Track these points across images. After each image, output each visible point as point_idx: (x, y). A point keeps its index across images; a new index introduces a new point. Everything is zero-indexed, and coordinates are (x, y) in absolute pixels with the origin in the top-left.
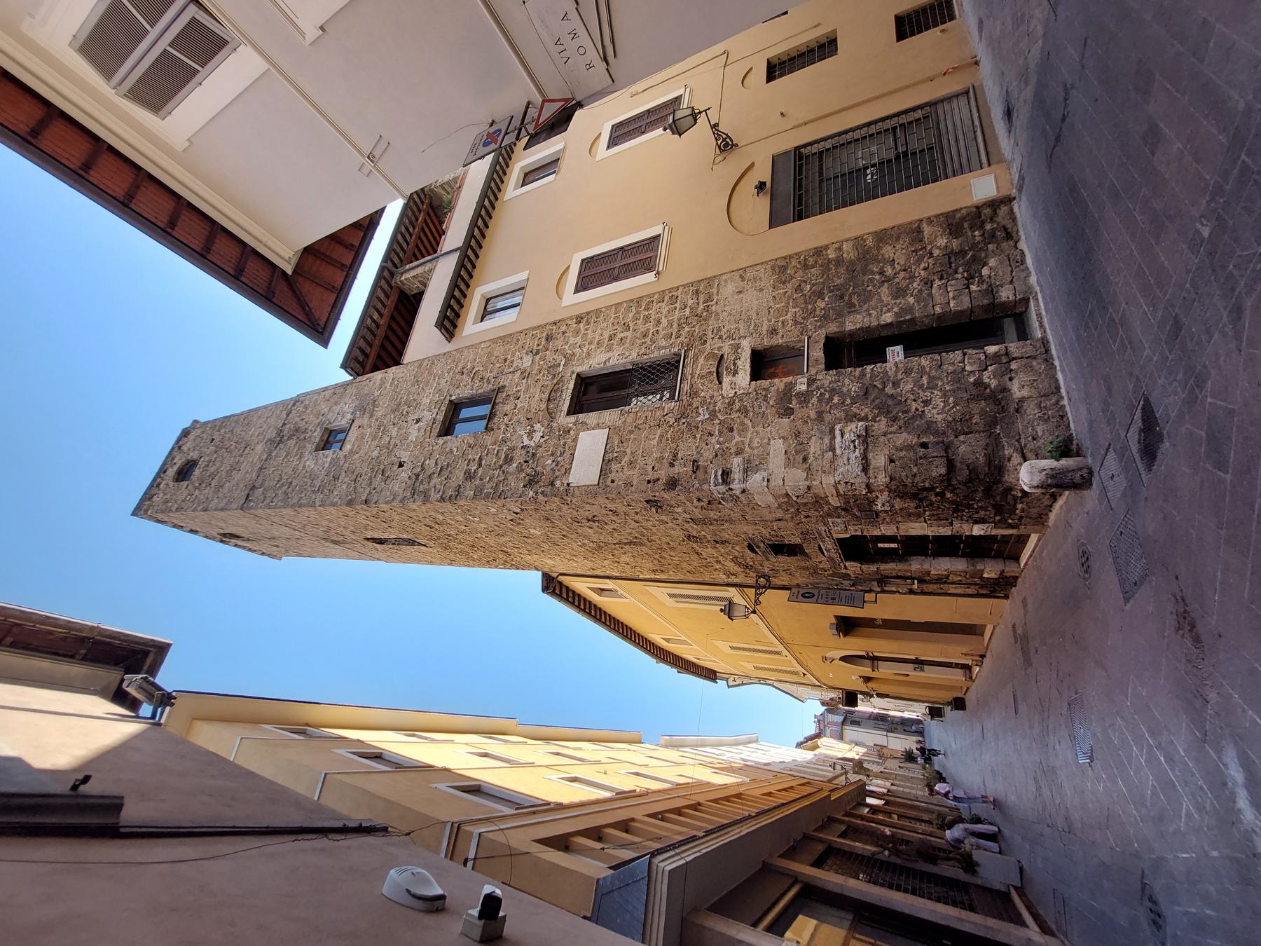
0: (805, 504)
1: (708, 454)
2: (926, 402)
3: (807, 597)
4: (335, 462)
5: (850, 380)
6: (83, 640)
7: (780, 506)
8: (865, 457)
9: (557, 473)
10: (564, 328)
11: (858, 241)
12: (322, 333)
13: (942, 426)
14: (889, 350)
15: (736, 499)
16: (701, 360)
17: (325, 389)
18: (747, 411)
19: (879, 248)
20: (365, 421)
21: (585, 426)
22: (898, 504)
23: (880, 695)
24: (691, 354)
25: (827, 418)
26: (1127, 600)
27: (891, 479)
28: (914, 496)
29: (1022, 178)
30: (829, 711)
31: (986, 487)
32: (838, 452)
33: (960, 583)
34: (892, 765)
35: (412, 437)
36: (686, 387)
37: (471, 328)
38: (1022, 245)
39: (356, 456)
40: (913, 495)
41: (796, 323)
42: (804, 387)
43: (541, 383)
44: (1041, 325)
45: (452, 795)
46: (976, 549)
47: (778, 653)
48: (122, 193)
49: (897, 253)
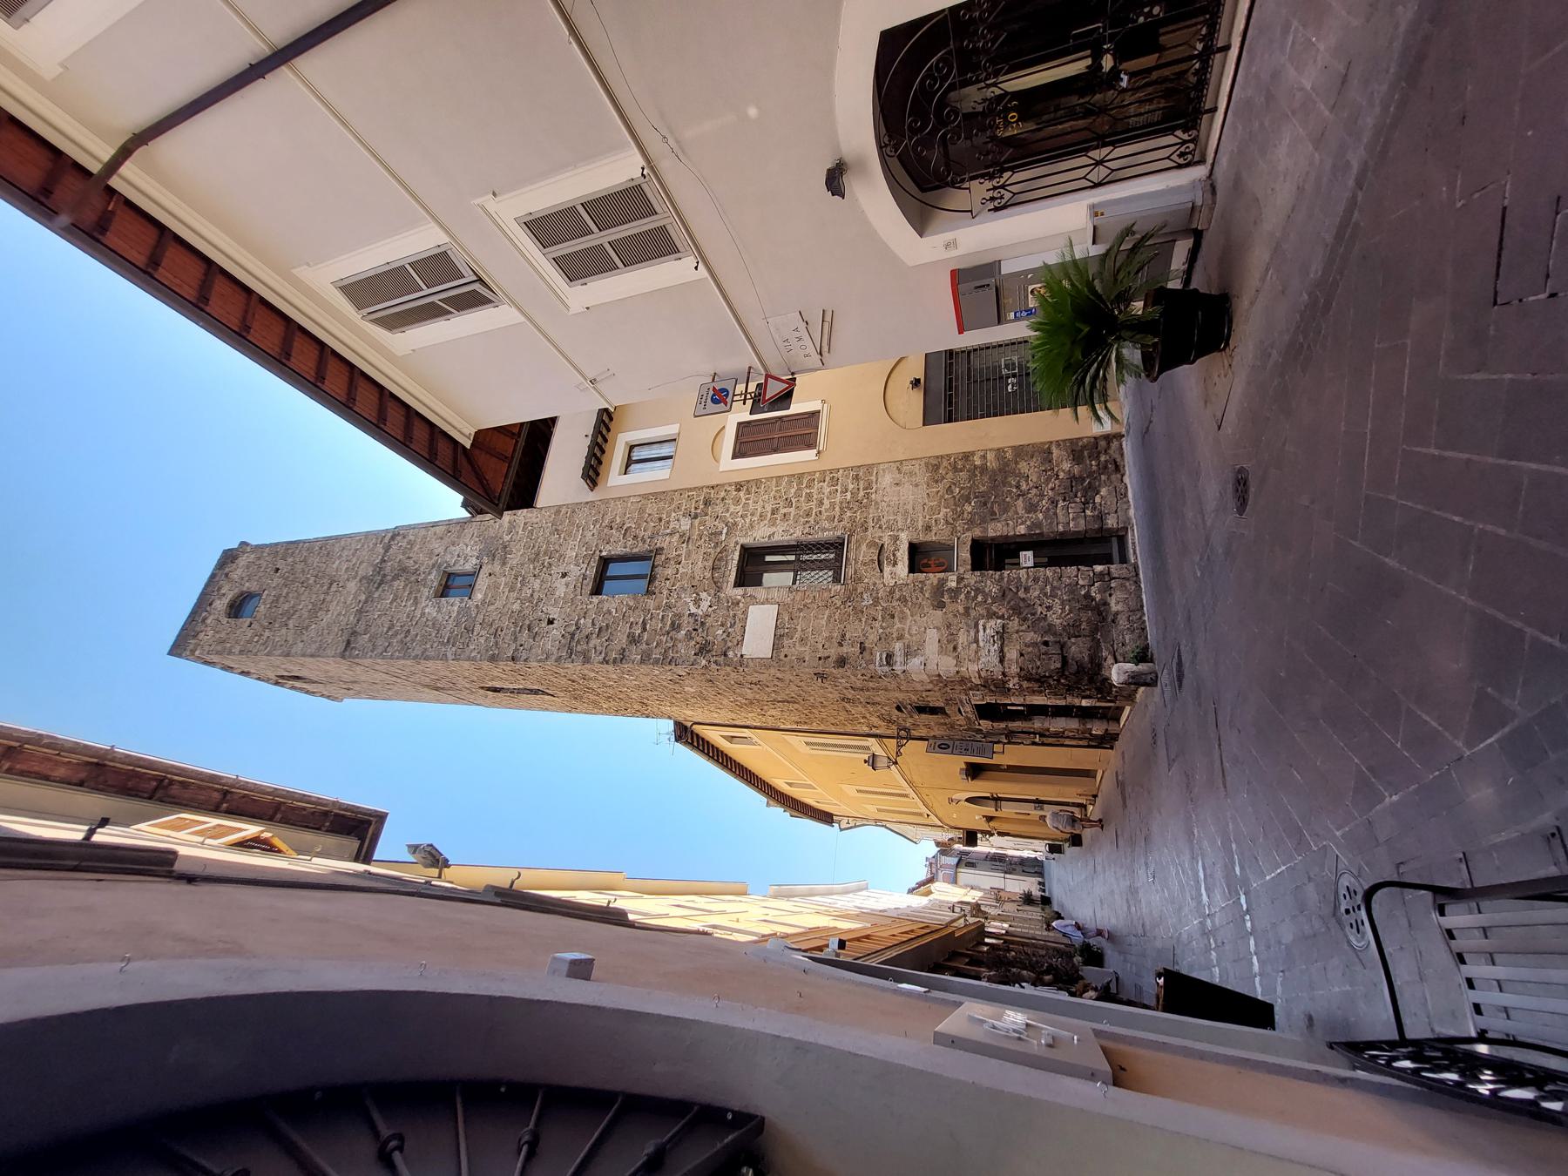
1: (873, 637)
2: (1049, 608)
3: (943, 747)
4: (464, 611)
5: (991, 582)
6: (326, 814)
8: (1001, 650)
10: (723, 494)
11: (1000, 452)
13: (1059, 629)
14: (1022, 554)
16: (864, 547)
17: (435, 524)
20: (497, 567)
21: (754, 600)
22: (1025, 684)
23: (1001, 834)
24: (853, 539)
25: (973, 614)
28: (1037, 681)
30: (943, 853)
31: (1090, 676)
33: (1073, 738)
34: (1010, 908)
36: (851, 572)
37: (614, 478)
38: (1127, 479)
39: (492, 608)
40: (1039, 681)
41: (947, 523)
42: (954, 584)
43: (703, 550)
46: (1086, 714)
47: (906, 796)
48: (193, 293)
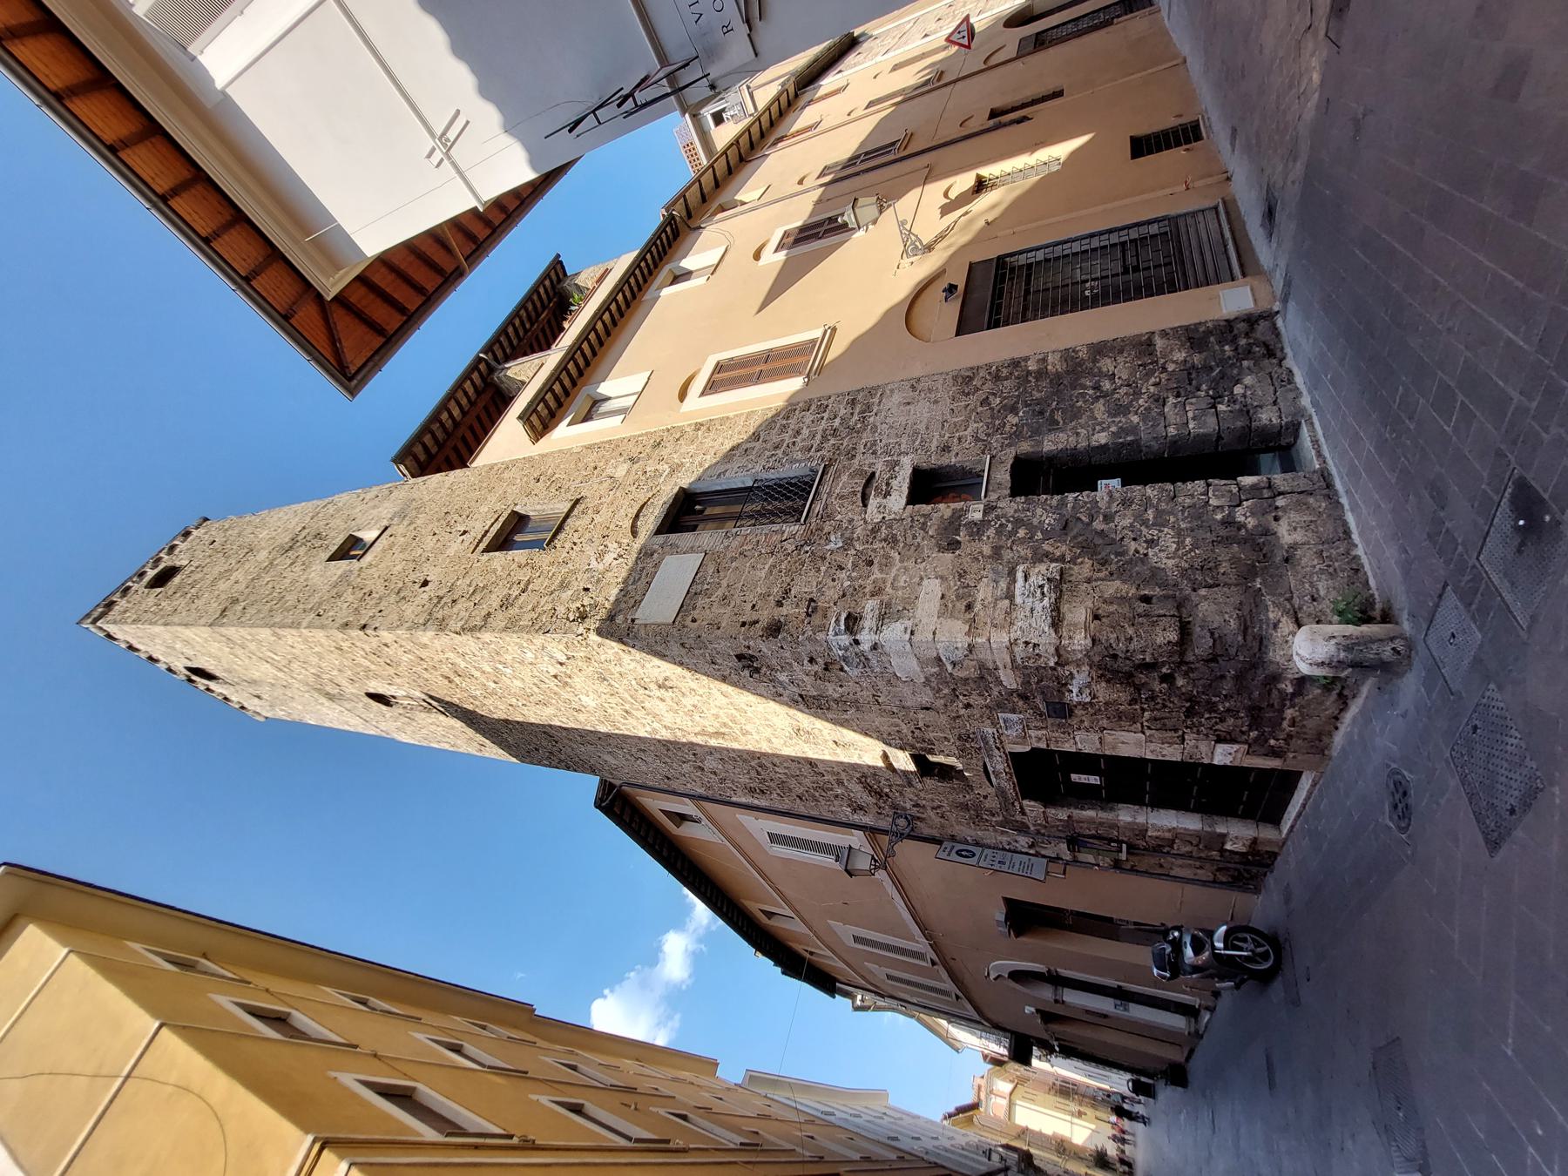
0: (966, 680)
1: (832, 593)
2: (1151, 543)
4: (345, 577)
5: (1044, 511)
7: (927, 682)
8: (1056, 608)
9: (623, 606)
11: (1068, 355)
12: (350, 379)
13: (1173, 575)
15: (864, 661)
16: (844, 478)
18: (895, 541)
19: (1095, 361)
21: (675, 549)
22: (1103, 692)
24: (832, 470)
25: (1007, 555)
26: (1494, 845)
27: (1094, 641)
28: (1127, 679)
29: (1288, 284)
32: (1018, 600)
35: (451, 552)
38: (1289, 362)
41: (977, 439)
42: (978, 516)
44: (1319, 454)
45: (354, 1095)
49: (1121, 368)
